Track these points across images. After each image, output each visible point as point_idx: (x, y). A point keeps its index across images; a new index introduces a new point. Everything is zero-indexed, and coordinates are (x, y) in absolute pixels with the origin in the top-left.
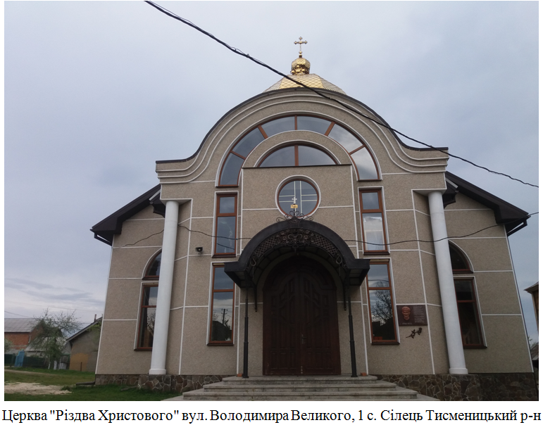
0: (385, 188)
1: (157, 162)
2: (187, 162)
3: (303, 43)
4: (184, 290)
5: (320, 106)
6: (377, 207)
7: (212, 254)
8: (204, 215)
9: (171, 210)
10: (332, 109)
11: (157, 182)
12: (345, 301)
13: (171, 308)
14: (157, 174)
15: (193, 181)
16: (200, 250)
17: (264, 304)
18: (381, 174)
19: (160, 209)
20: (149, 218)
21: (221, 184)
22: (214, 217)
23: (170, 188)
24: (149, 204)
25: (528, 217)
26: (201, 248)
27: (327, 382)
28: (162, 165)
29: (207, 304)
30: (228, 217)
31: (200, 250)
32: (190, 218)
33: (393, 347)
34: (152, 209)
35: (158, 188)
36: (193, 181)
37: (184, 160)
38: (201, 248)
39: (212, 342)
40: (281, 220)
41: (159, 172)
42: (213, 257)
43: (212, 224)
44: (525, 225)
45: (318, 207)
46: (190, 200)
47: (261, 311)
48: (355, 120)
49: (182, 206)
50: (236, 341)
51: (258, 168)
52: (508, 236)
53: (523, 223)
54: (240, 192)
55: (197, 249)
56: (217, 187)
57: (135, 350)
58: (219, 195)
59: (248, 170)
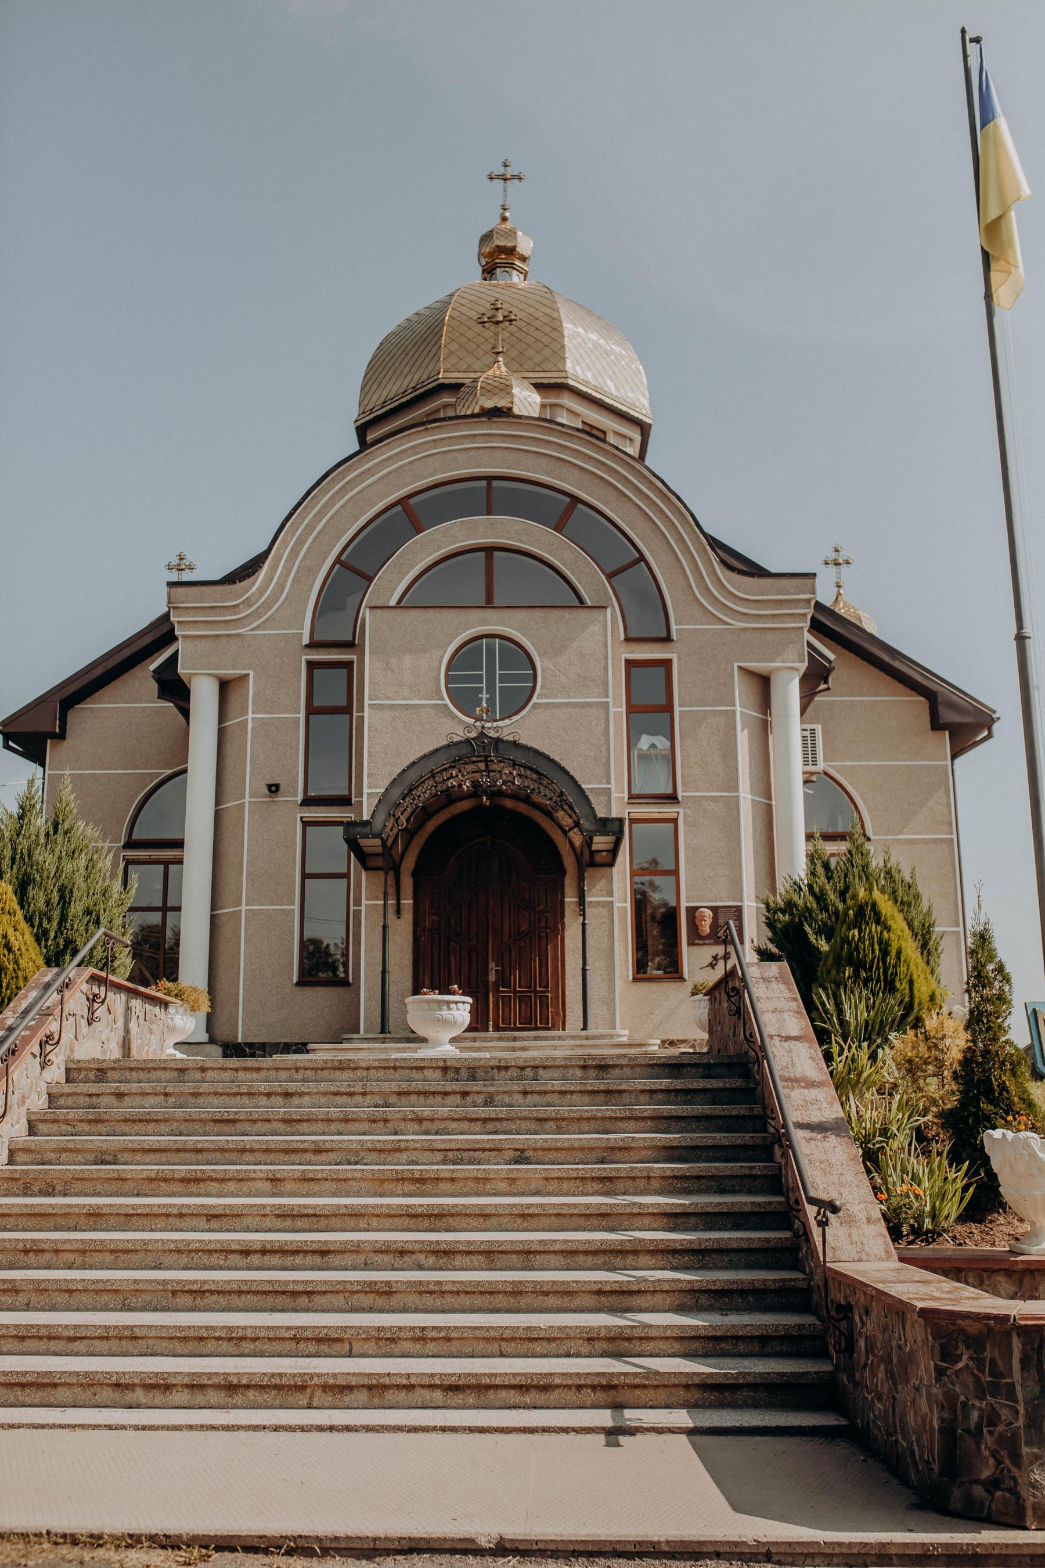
0: (679, 658)
3: (513, 177)
5: (545, 460)
6: (663, 702)
8: (274, 713)
10: (572, 469)
13: (212, 909)
15: (253, 630)
17: (414, 904)
18: (674, 627)
21: (317, 638)
22: (302, 716)
25: (993, 721)
27: (536, 1039)
28: (180, 590)
29: (293, 903)
31: (274, 789)
32: (251, 716)
33: (678, 984)
36: (253, 630)
38: (277, 786)
39: (305, 979)
40: (456, 739)
42: (302, 805)
43: (298, 730)
44: (990, 736)
45: (534, 700)
46: (248, 674)
47: (408, 916)
48: (623, 499)
49: (225, 686)
50: (357, 978)
51: (398, 605)
52: (954, 757)
53: (986, 733)
54: (362, 660)
55: (269, 786)
56: (307, 646)
57: (297, 984)
58: (312, 665)
59: (379, 611)
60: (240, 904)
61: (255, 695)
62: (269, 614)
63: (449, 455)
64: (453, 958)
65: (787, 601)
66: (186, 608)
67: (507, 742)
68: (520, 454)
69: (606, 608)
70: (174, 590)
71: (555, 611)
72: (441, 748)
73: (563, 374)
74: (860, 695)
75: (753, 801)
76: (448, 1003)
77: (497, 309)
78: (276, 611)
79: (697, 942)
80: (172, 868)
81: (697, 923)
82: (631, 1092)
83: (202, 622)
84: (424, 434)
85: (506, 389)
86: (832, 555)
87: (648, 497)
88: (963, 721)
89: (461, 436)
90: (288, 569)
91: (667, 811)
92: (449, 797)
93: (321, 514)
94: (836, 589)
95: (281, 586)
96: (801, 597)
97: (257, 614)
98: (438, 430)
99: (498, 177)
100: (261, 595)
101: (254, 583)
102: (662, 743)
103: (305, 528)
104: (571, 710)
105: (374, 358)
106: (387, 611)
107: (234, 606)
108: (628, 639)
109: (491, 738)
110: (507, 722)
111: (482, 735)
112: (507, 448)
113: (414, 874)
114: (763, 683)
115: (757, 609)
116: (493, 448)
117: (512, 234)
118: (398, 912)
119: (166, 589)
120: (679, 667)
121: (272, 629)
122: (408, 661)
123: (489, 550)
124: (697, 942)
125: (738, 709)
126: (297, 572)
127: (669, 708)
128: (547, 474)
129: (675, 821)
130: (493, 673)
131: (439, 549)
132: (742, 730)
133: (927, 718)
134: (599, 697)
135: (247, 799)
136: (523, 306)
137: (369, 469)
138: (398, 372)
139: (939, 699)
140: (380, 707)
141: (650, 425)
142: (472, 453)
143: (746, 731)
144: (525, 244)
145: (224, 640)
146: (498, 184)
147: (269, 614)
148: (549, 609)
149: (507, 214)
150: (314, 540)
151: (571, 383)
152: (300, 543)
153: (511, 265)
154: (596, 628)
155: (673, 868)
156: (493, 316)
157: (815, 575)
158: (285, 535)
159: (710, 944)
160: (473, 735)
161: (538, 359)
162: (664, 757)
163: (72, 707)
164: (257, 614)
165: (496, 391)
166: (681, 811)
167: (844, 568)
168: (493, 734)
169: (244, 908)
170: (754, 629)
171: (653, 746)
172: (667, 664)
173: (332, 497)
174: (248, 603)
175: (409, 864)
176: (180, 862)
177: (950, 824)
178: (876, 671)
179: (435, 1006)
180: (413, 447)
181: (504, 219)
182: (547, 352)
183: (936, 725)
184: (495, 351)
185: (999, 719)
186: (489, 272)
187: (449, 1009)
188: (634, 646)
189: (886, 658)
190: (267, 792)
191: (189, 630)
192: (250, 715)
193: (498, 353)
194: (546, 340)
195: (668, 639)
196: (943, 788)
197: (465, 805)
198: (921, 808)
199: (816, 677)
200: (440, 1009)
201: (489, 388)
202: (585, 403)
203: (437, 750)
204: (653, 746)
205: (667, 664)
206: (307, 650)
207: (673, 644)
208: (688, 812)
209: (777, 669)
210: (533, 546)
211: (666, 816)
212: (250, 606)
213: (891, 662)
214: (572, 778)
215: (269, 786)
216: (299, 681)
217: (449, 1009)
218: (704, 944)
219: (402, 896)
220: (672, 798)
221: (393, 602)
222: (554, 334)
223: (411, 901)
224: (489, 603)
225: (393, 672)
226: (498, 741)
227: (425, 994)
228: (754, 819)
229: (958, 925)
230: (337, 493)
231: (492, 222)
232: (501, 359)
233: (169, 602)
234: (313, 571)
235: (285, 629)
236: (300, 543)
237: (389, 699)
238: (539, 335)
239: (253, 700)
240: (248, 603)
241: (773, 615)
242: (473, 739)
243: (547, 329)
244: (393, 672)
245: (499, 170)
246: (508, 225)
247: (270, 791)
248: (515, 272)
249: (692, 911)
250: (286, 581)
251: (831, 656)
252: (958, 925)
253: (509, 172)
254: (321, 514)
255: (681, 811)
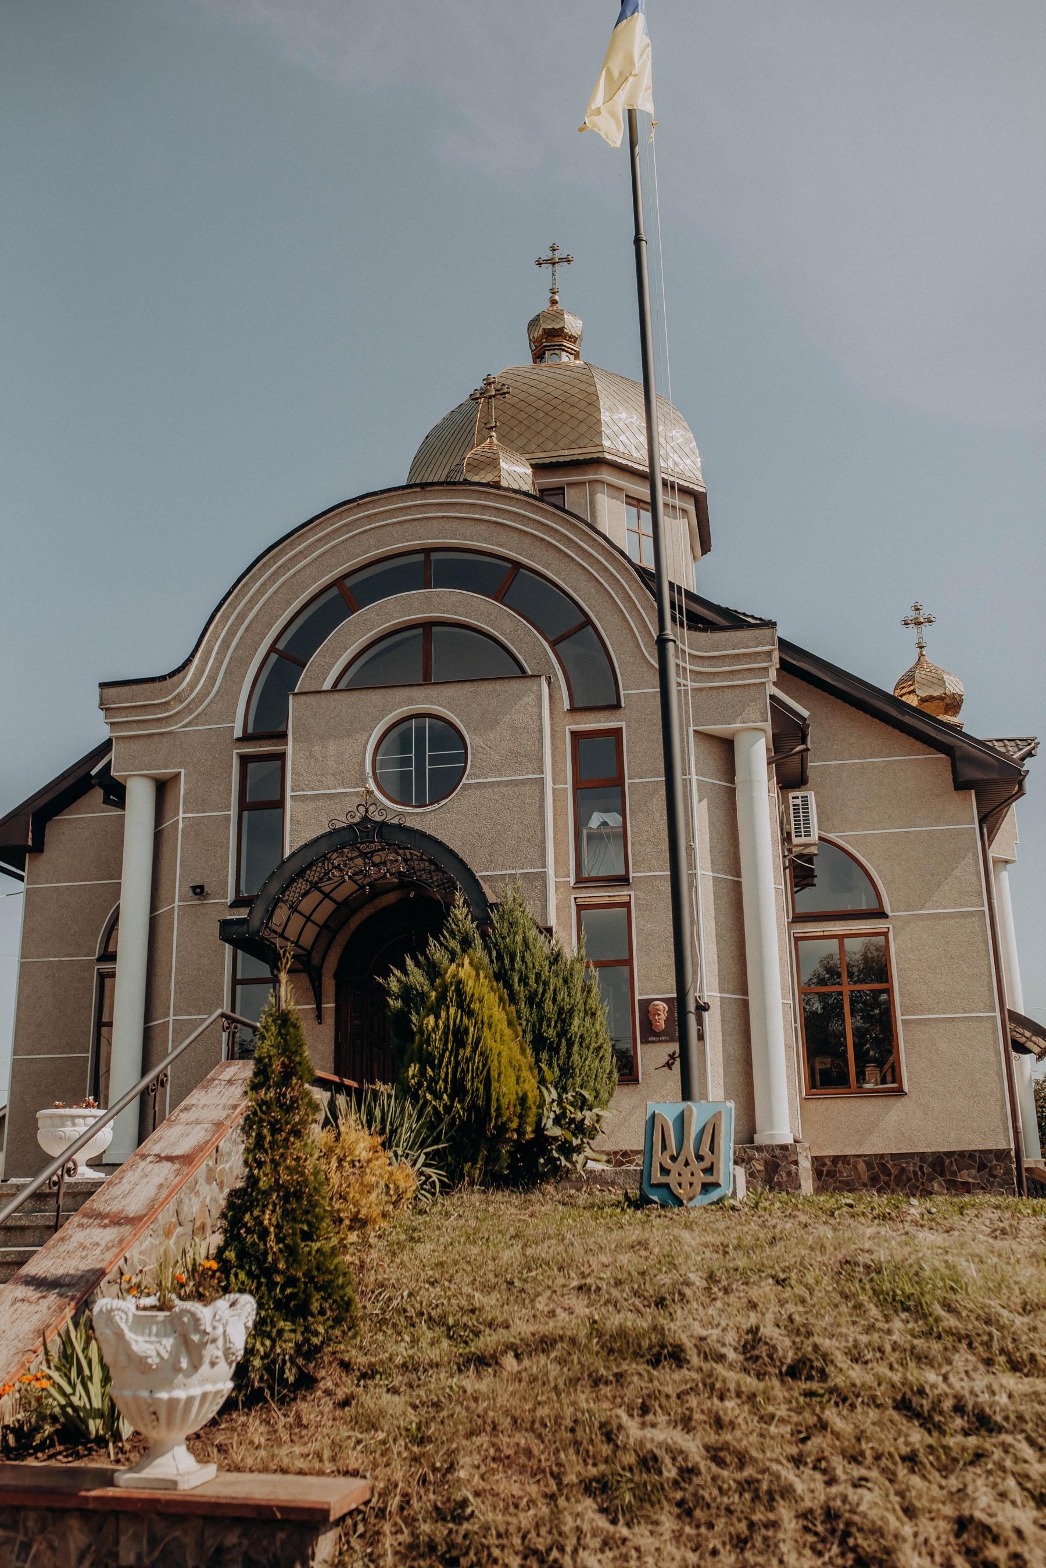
0: (628, 726)
1: (103, 685)
2: (169, 681)
4: (170, 982)
5: (483, 526)
7: (230, 898)
8: (209, 811)
9: (140, 796)
10: (511, 534)
11: (102, 732)
12: (319, 1003)
14: (102, 713)
15: (185, 726)
16: (199, 891)
19: (116, 794)
20: (91, 811)
23: (134, 747)
24: (89, 782)
26: (202, 887)
28: (112, 691)
30: (261, 805)
31: (199, 891)
32: (181, 816)
33: (631, 1087)
34: (98, 794)
35: (106, 747)
36: (185, 726)
37: (163, 678)
38: (202, 887)
41: (107, 709)
42: (231, 906)
43: (228, 828)
44: (1021, 792)
45: (464, 781)
47: (330, 1021)
49: (163, 788)
51: (334, 689)
55: (194, 888)
56: (238, 740)
58: (245, 759)
60: (168, 1015)
61: (186, 794)
62: (201, 708)
63: (383, 530)
64: (376, 1066)
65: (745, 655)
66: (119, 708)
67: (393, 826)
68: (456, 523)
69: (540, 676)
70: (106, 691)
71: (486, 683)
72: (323, 836)
73: (600, 449)
74: (872, 756)
75: (714, 877)
76: (73, 1117)
77: (490, 384)
78: (208, 705)
79: (651, 1039)
80: (108, 981)
81: (651, 1018)
82: (36, 1227)
83: (134, 721)
84: (356, 510)
85: (493, 463)
86: (913, 614)
87: (591, 555)
88: (985, 777)
89: (395, 509)
90: (219, 661)
91: (618, 894)
92: (377, 890)
93: (252, 602)
94: (919, 650)
95: (212, 680)
96: (759, 649)
97: (189, 710)
98: (370, 505)
99: (546, 261)
100: (192, 689)
101: (184, 678)
102: (614, 819)
103: (237, 618)
104: (503, 789)
105: (419, 452)
106: (323, 696)
107: (165, 703)
108: (573, 710)
109: (374, 822)
110: (436, 806)
111: (366, 819)
112: (443, 517)
113: (336, 976)
114: (725, 748)
115: (711, 666)
116: (429, 518)
117: (559, 315)
118: (319, 1017)
119: (99, 690)
120: (629, 735)
121: (204, 725)
122: (332, 746)
123: (427, 626)
124: (651, 1039)
125: (694, 777)
126: (229, 663)
127: (619, 782)
128: (486, 541)
129: (627, 905)
130: (430, 757)
131: (372, 629)
132: (700, 801)
133: (949, 776)
134: (534, 773)
135: (177, 903)
136: (557, 384)
137: (301, 552)
138: (438, 463)
139: (958, 754)
140: (303, 798)
141: (705, 494)
142: (407, 526)
143: (705, 802)
144: (573, 324)
145: (156, 739)
146: (547, 269)
147: (201, 708)
148: (480, 683)
149: (557, 297)
150: (246, 630)
151: (609, 457)
152: (231, 633)
153: (561, 348)
154: (529, 699)
155: (627, 957)
156: (487, 391)
157: (775, 624)
158: (216, 627)
159: (666, 1041)
160: (357, 820)
161: (573, 436)
162: (616, 836)
163: (50, 819)
164: (189, 710)
165: (481, 466)
166: (632, 893)
167: (926, 628)
168: (378, 818)
169: (171, 1018)
170: (710, 688)
171: (605, 824)
172: (618, 731)
173: (264, 584)
174: (179, 699)
175: (331, 964)
176: (113, 975)
177: (980, 894)
178: (889, 728)
179: (58, 1121)
180: (345, 525)
181: (554, 302)
182: (582, 428)
183: (961, 785)
184: (488, 426)
185: (1027, 772)
186: (538, 356)
187: (74, 1125)
188: (578, 716)
189: (894, 712)
190: (191, 894)
191: (121, 731)
192: (181, 815)
193: (492, 428)
194: (581, 416)
195: (617, 706)
196: (970, 855)
197: (391, 898)
198: (946, 878)
199: (788, 735)
200: (63, 1125)
201: (475, 463)
202: (627, 476)
203: (318, 838)
204: (605, 824)
205: (618, 731)
206: (238, 744)
207: (621, 712)
208: (639, 893)
209: (739, 731)
210: (470, 618)
211: (617, 900)
212: (181, 702)
213: (899, 717)
214: (461, 861)
215: (194, 888)
216: (230, 776)
217: (74, 1125)
218: (659, 1041)
219: (324, 999)
220: (623, 880)
221: (327, 685)
222: (589, 409)
223: (333, 1005)
224: (427, 680)
225: (316, 760)
226: (383, 824)
227: (57, 1107)
228: (716, 898)
229: (993, 1010)
230: (269, 578)
231: (545, 306)
232: (494, 434)
233: (101, 704)
234: (246, 662)
235: (216, 723)
236: (231, 633)
237: (312, 789)
238: (573, 411)
239: (185, 799)
240: (179, 699)
241: (731, 672)
242: (355, 824)
243: (583, 404)
244: (316, 760)
245: (547, 254)
246: (559, 306)
247: (195, 894)
248: (564, 354)
249: (645, 1004)
250: (217, 674)
251: (805, 713)
252: (993, 1010)
253: (558, 255)
254: (252, 602)
255: (632, 893)
